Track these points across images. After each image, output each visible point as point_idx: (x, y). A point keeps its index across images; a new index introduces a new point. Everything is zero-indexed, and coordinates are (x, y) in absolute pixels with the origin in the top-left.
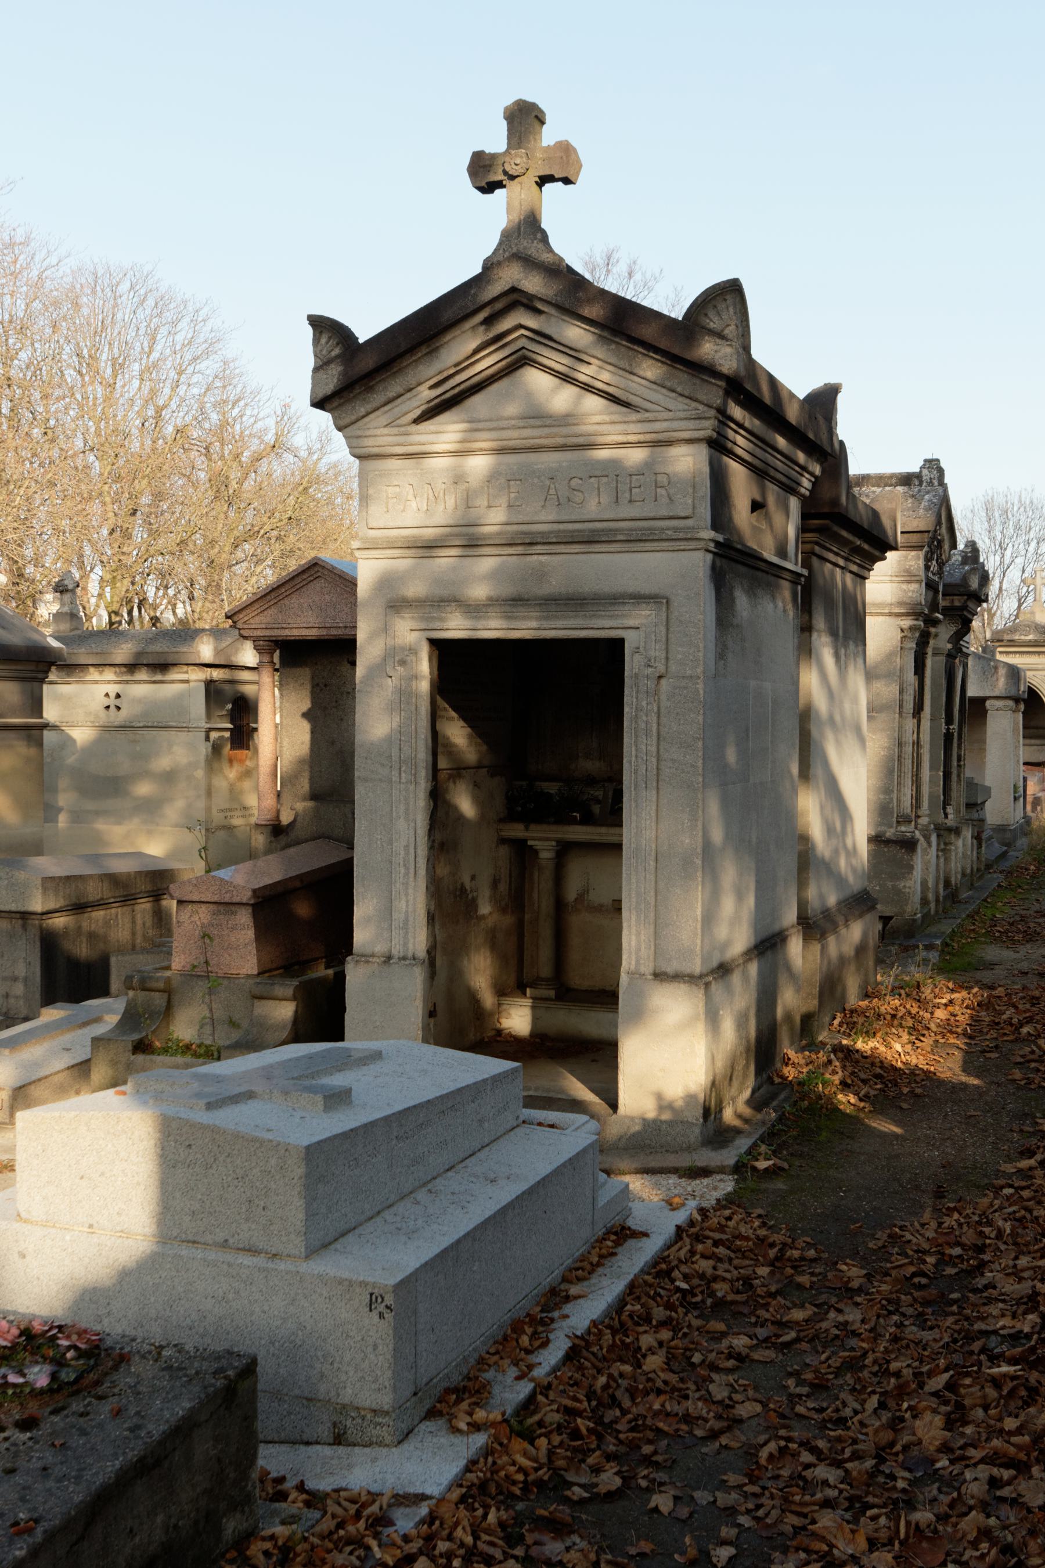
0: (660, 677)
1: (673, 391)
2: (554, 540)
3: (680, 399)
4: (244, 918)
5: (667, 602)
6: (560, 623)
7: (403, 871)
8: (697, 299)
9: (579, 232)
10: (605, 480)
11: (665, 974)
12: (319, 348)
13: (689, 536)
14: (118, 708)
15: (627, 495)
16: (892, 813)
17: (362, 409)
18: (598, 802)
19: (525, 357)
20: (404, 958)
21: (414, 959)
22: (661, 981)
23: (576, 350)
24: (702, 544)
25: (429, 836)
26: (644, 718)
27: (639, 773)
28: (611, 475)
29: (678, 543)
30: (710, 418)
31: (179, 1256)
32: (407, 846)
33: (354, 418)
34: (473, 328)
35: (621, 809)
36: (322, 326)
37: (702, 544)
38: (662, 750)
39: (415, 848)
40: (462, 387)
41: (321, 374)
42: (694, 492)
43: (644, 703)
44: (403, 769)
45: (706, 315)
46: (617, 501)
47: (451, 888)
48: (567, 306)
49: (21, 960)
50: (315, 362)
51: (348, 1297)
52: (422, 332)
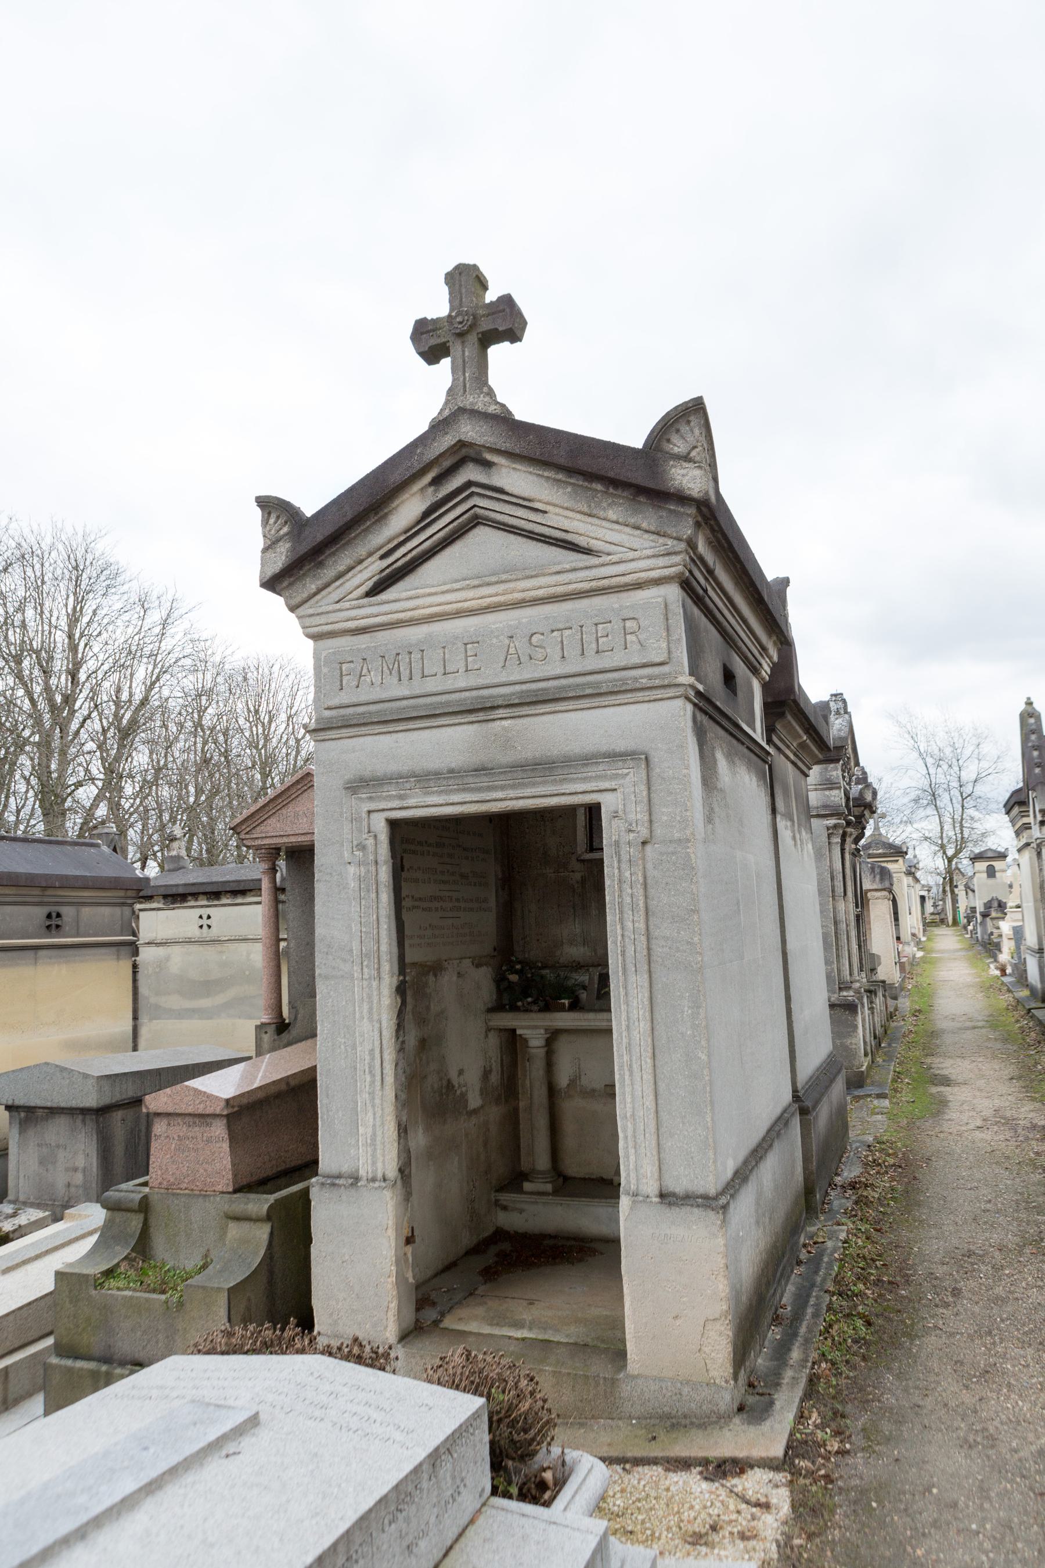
0: (644, 843)
1: (638, 528)
2: (517, 701)
3: (646, 536)
4: (219, 1130)
5: (646, 758)
7: (368, 1079)
8: (652, 432)
9: (524, 382)
10: (567, 633)
11: (673, 1195)
12: (268, 528)
13: (666, 682)
14: (209, 927)
15: (594, 646)
16: (834, 981)
17: (313, 586)
18: (584, 988)
19: (476, 516)
20: (374, 1180)
21: (385, 1180)
22: (670, 1204)
23: (529, 500)
24: (681, 691)
25: (397, 1037)
26: (629, 891)
27: (627, 954)
28: (574, 627)
29: (655, 692)
30: (681, 552)
32: (373, 1050)
33: (305, 595)
34: (422, 489)
35: (608, 994)
36: (269, 505)
37: (681, 691)
38: (651, 927)
40: (414, 553)
41: (270, 554)
42: (668, 635)
43: (627, 874)
44: (365, 963)
45: (668, 441)
46: (583, 654)
47: (436, 1086)
49: (81, 1152)
52: (368, 501)
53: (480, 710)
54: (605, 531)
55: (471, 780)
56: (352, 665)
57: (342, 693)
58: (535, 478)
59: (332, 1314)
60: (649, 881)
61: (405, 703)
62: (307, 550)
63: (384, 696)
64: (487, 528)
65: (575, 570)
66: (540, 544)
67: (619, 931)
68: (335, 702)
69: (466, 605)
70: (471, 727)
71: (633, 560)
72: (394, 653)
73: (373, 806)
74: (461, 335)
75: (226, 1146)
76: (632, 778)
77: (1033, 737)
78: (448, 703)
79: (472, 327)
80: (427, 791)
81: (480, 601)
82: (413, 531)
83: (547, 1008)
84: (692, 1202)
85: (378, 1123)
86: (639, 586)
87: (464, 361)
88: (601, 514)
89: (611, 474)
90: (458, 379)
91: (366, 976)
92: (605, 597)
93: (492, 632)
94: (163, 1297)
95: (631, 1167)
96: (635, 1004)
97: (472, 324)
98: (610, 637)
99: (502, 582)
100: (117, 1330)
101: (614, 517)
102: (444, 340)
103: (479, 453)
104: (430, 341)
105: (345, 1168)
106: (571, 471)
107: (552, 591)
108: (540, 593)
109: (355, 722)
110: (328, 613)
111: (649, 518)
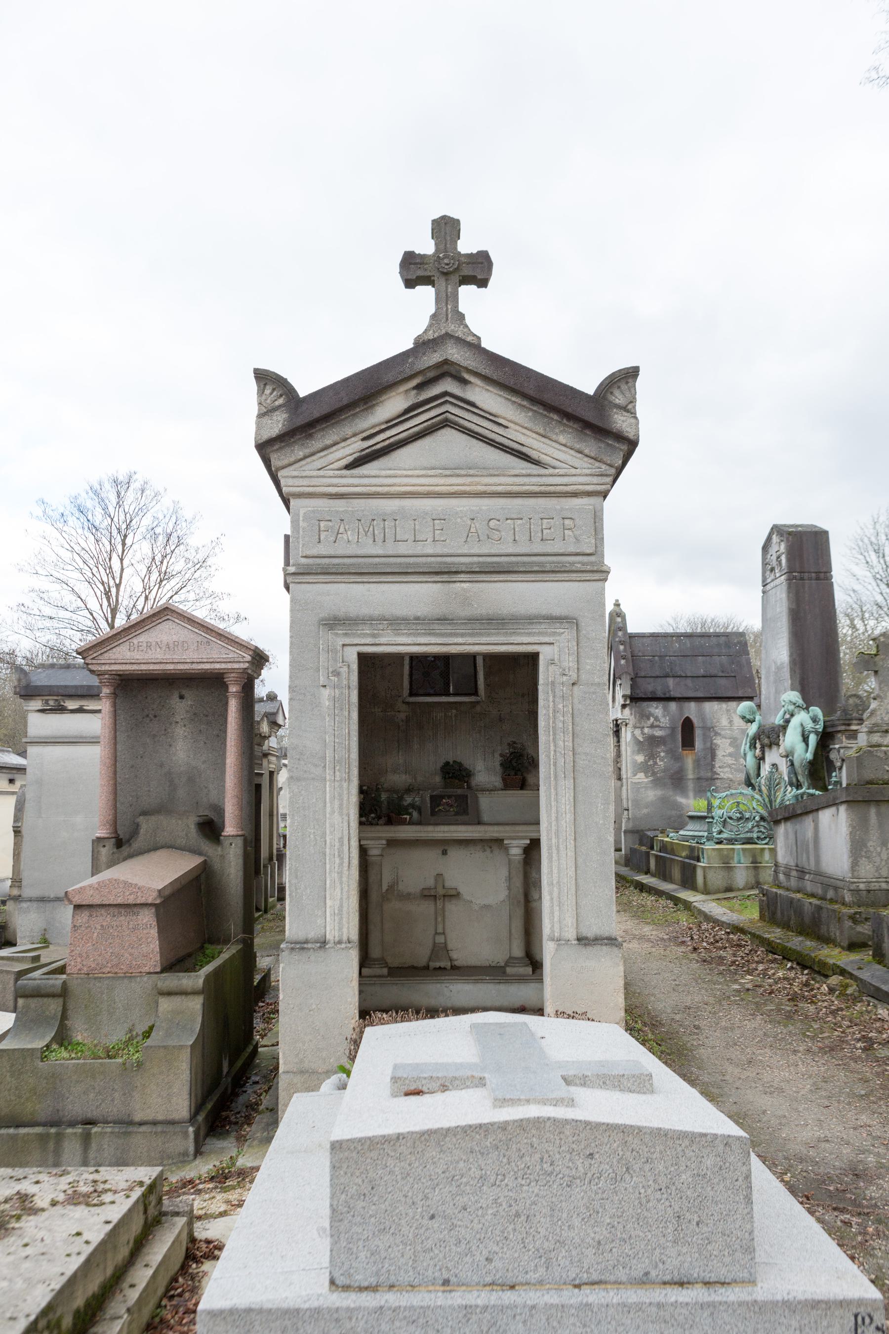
0: (573, 684)
1: (580, 452)
2: (477, 569)
3: (586, 459)
4: (148, 918)
6: (484, 640)
7: (337, 861)
10: (519, 522)
11: (586, 938)
13: (595, 568)
15: (540, 535)
19: (446, 420)
20: (340, 942)
22: (585, 945)
26: (562, 719)
27: (558, 765)
29: (585, 575)
31: (587, 1305)
33: (292, 459)
36: (265, 379)
39: (349, 840)
40: (392, 440)
41: (266, 420)
42: (596, 534)
43: (560, 706)
44: (337, 768)
45: (612, 393)
48: (495, 378)
50: (259, 410)
51: (825, 1323)
53: (445, 572)
54: (553, 450)
55: (436, 627)
56: (330, 524)
57: (321, 546)
58: (503, 400)
59: (297, 1055)
60: (575, 712)
61: (377, 560)
62: (299, 424)
63: (360, 552)
64: (453, 430)
65: (529, 475)
66: (498, 451)
67: (552, 748)
68: (314, 552)
69: (437, 489)
70: (434, 585)
71: (574, 475)
72: (371, 518)
73: (347, 641)
74: (446, 274)
75: (154, 932)
76: (565, 637)
77: (620, 633)
78: (417, 565)
79: (457, 270)
80: (397, 632)
81: (448, 488)
82: (394, 422)
83: (390, 822)
84: (600, 942)
85: (345, 897)
86: (575, 495)
87: (447, 295)
88: (554, 437)
89: (570, 410)
90: (442, 308)
91: (338, 778)
92: (548, 499)
93: (457, 513)
94: (120, 1060)
95: (556, 919)
96: (563, 801)
97: (447, 266)
98: (552, 530)
99: (470, 476)
100: (67, 1095)
101: (564, 442)
102: (429, 274)
103: (459, 372)
104: (414, 270)
105: (311, 935)
106: (533, 400)
107: (509, 488)
108: (500, 489)
109: (334, 570)
110: (311, 477)
111: (591, 446)
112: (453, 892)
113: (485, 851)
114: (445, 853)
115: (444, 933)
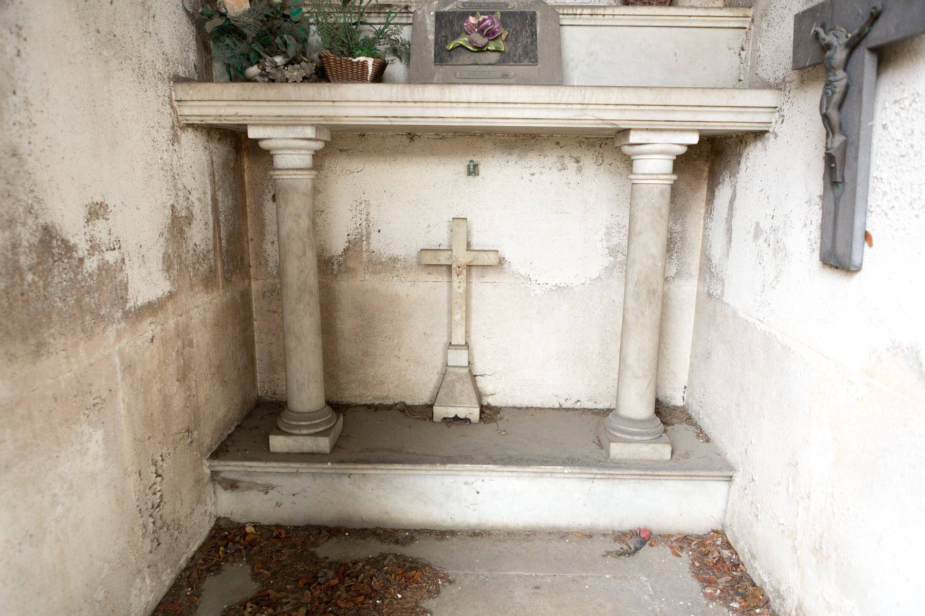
83: (321, 75)
96: (223, 241)
112: (491, 259)
113: (564, 168)
114: (473, 170)
115: (467, 345)
